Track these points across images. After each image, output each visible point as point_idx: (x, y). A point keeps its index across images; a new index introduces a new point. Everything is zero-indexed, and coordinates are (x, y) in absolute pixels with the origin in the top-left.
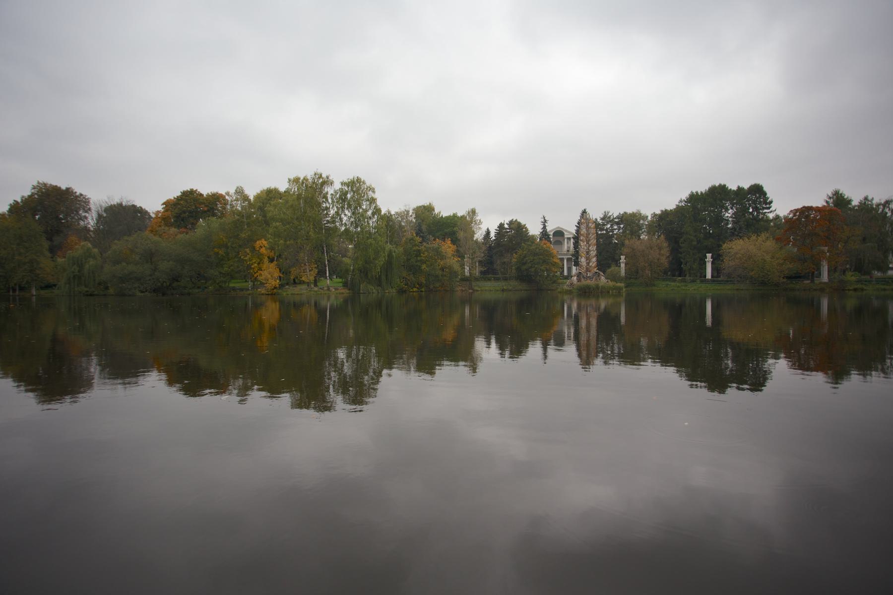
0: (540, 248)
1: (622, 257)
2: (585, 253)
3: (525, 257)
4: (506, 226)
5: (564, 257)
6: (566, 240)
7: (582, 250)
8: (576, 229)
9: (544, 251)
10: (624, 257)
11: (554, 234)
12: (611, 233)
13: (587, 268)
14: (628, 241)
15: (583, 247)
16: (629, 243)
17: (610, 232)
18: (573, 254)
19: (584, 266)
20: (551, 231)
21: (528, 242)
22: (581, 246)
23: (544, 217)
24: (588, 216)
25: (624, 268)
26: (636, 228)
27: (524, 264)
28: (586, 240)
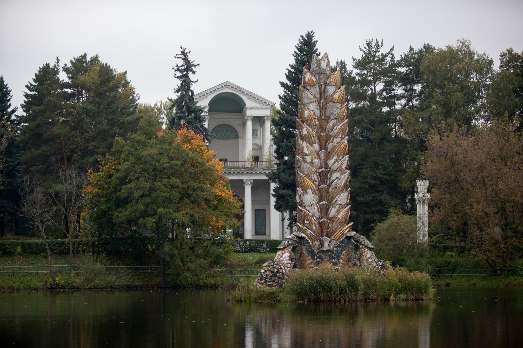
0: (172, 152)
1: (419, 183)
2: (315, 177)
3: (123, 181)
4: (63, 77)
5: (244, 178)
6: (249, 124)
7: (305, 167)
8: (282, 94)
9: (185, 163)
10: (427, 183)
11: (212, 103)
12: (385, 109)
13: (321, 224)
14: (437, 137)
15: (308, 159)
16: (440, 144)
17: (383, 104)
18: (274, 174)
19: (313, 219)
20: (203, 95)
21: (134, 131)
22: (303, 155)
23: (183, 53)
24: (323, 65)
25: (426, 220)
26: (459, 94)
27: (121, 203)
28: (319, 138)
